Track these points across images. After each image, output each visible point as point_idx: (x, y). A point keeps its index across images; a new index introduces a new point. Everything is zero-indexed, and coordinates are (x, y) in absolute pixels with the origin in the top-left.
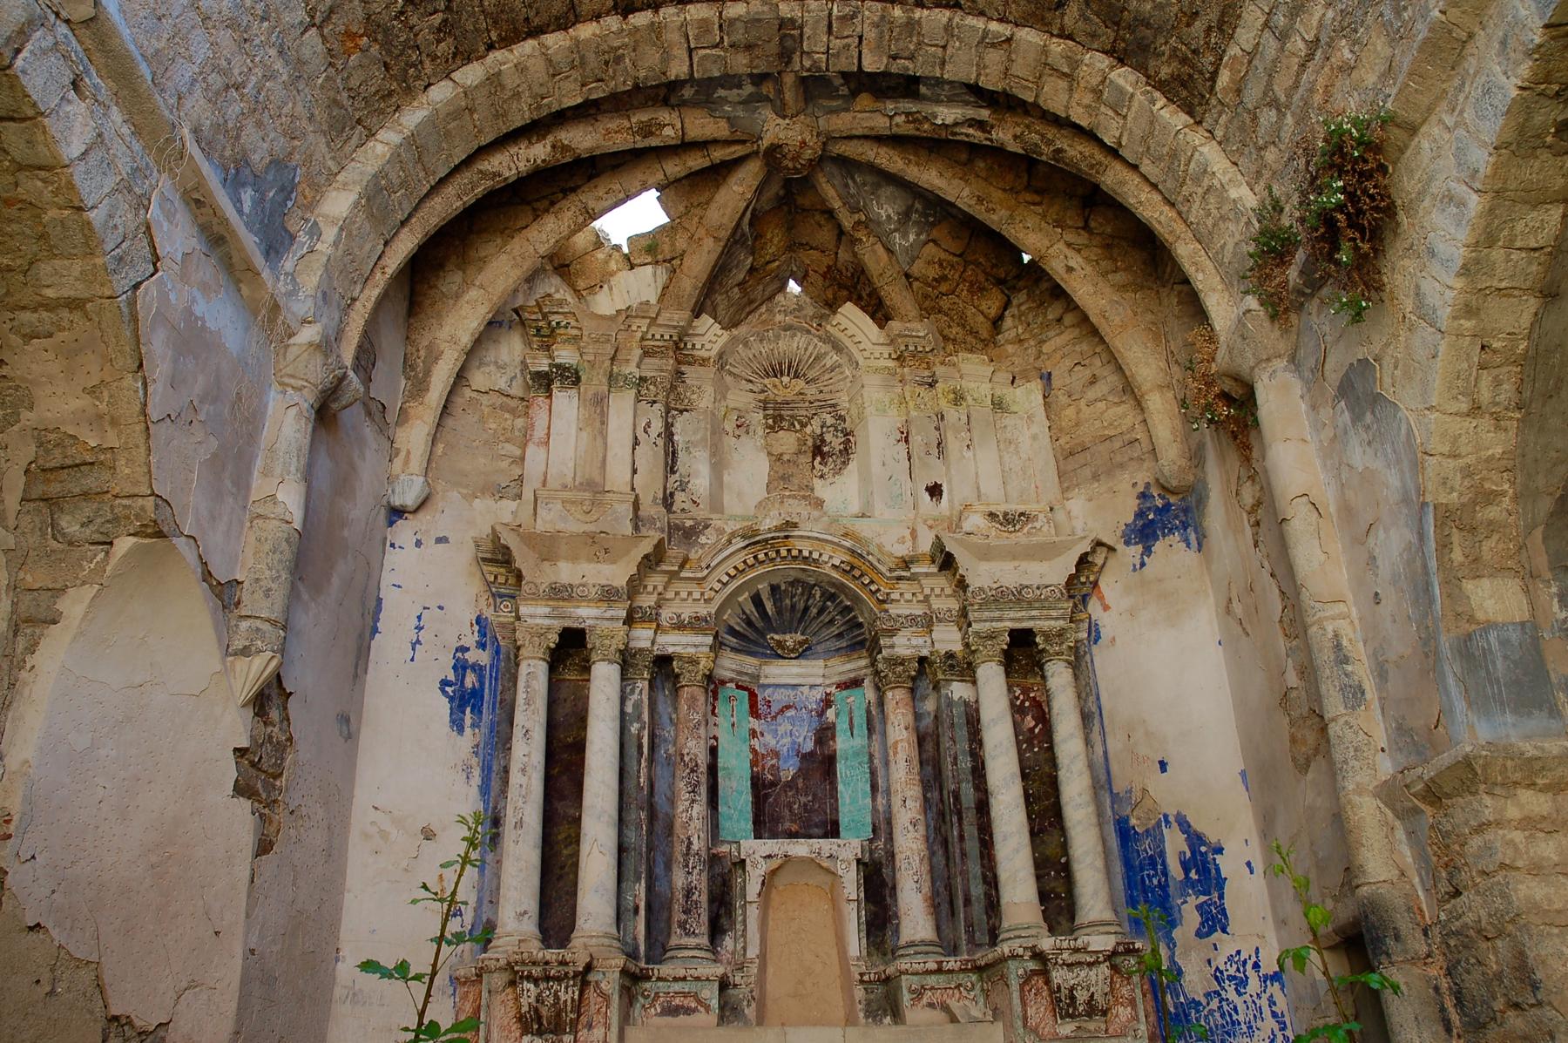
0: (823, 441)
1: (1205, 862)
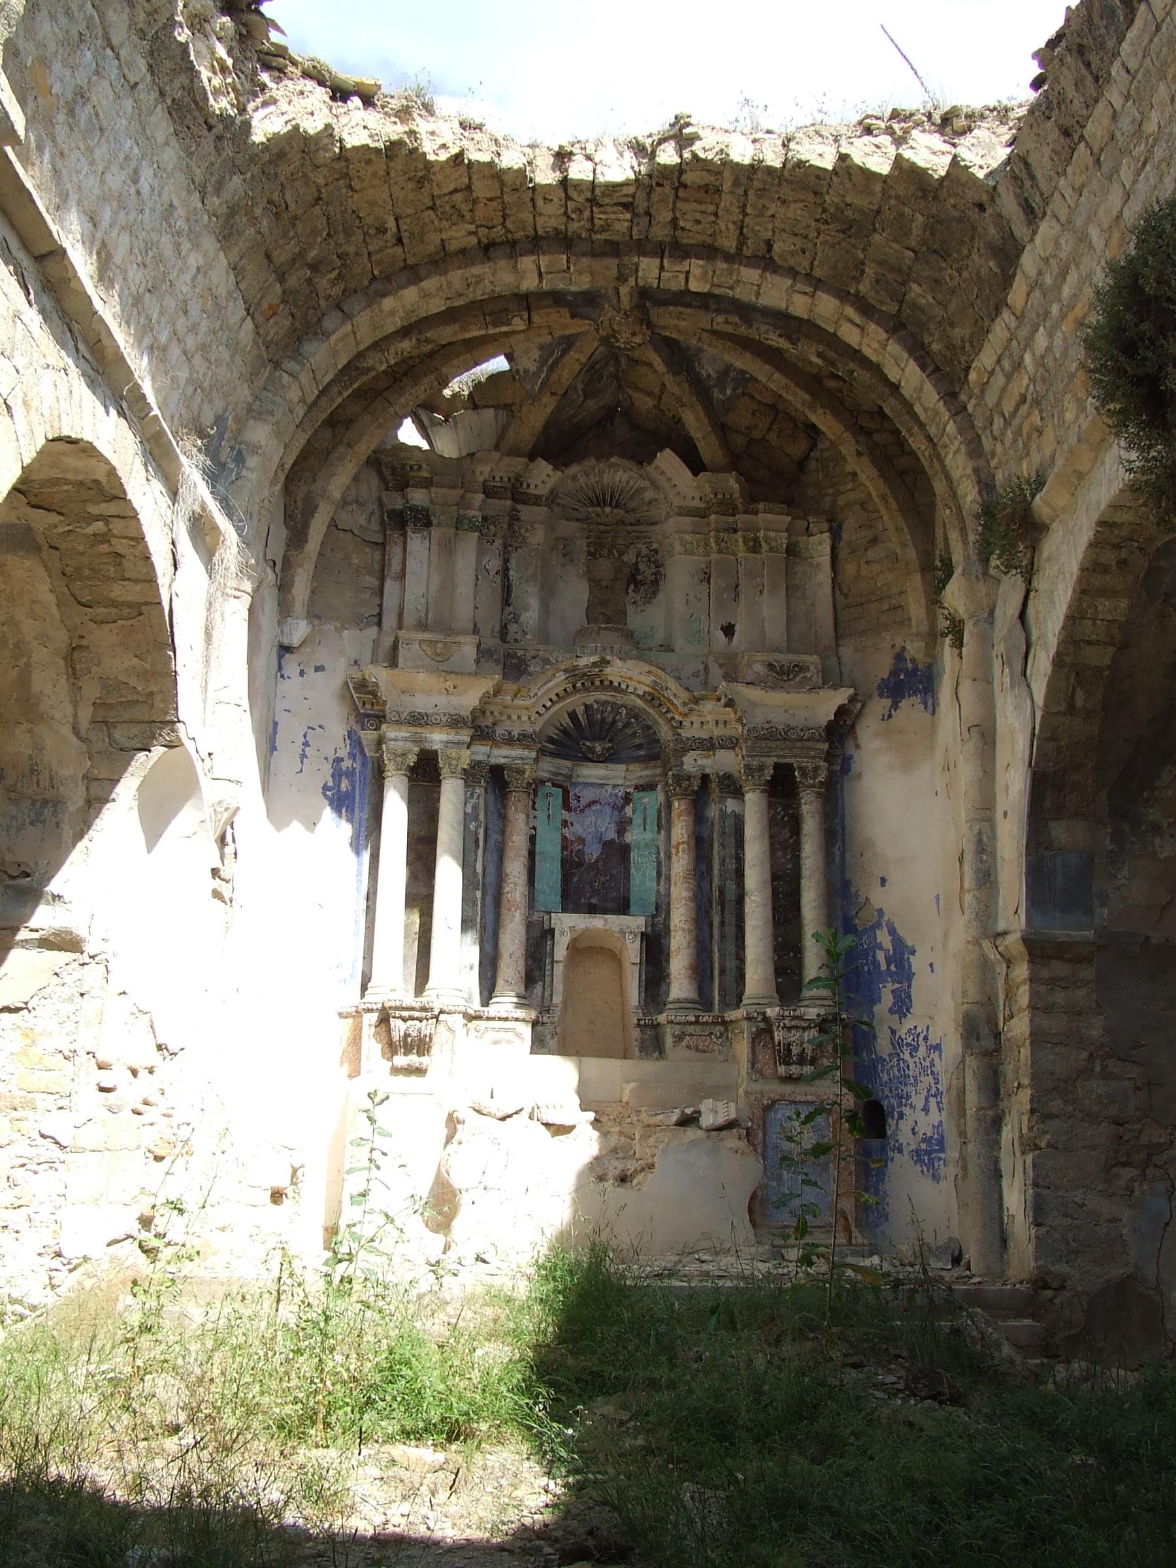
0: (637, 570)
1: (902, 959)
